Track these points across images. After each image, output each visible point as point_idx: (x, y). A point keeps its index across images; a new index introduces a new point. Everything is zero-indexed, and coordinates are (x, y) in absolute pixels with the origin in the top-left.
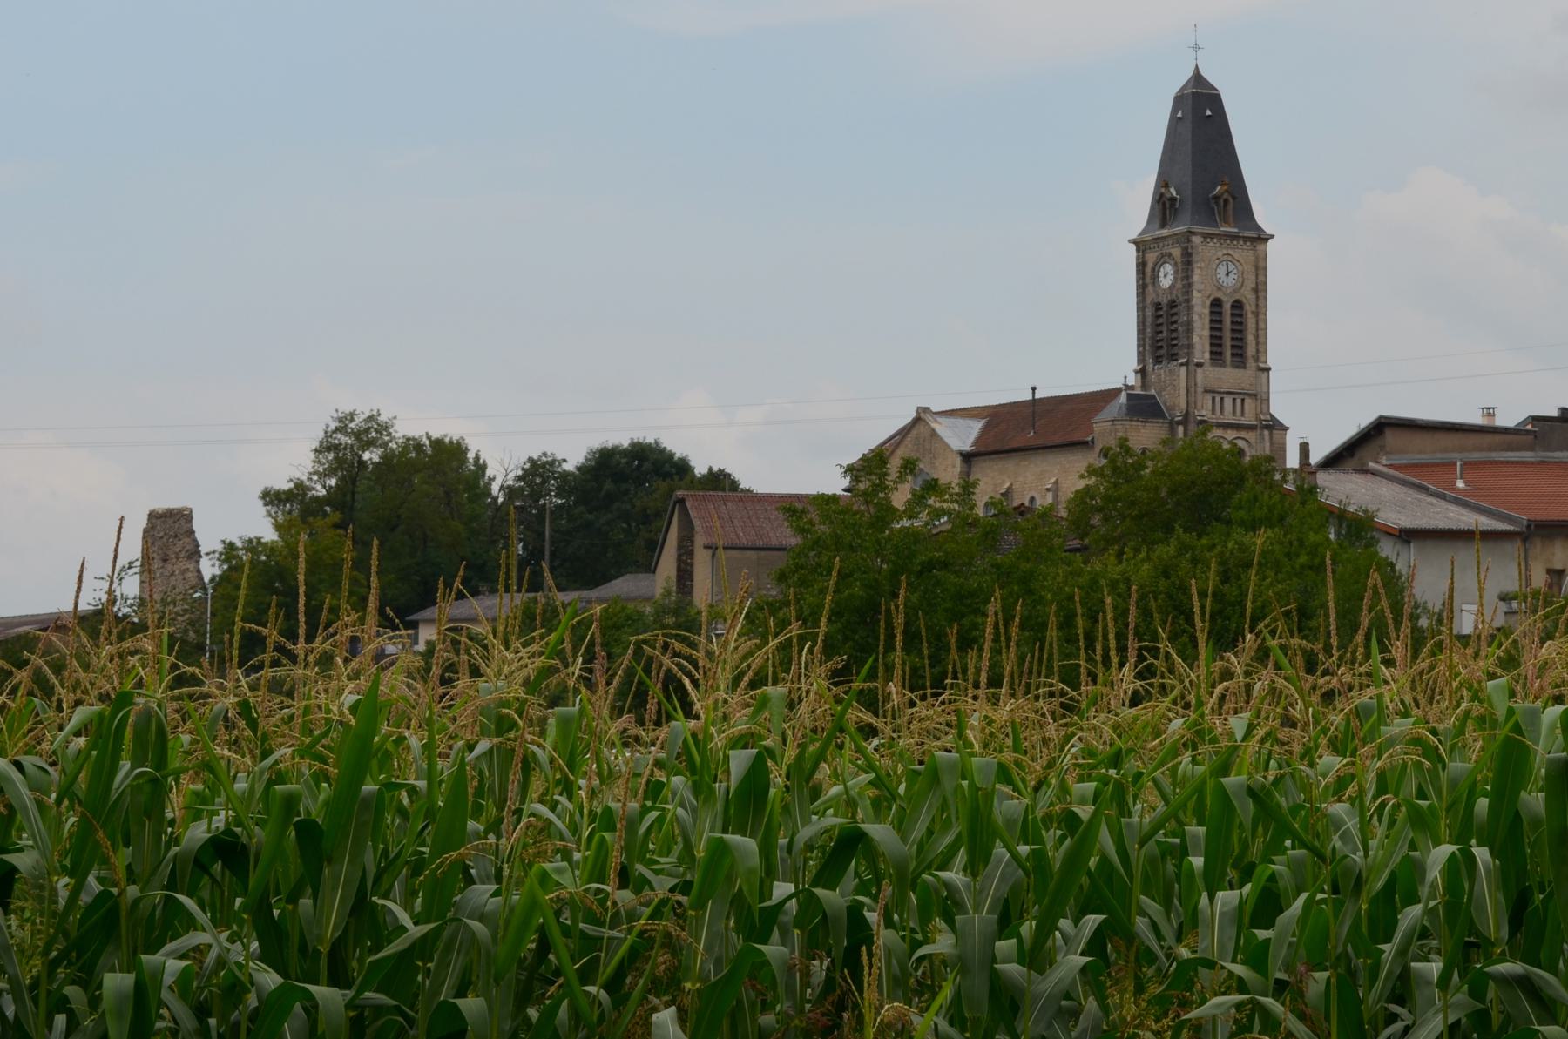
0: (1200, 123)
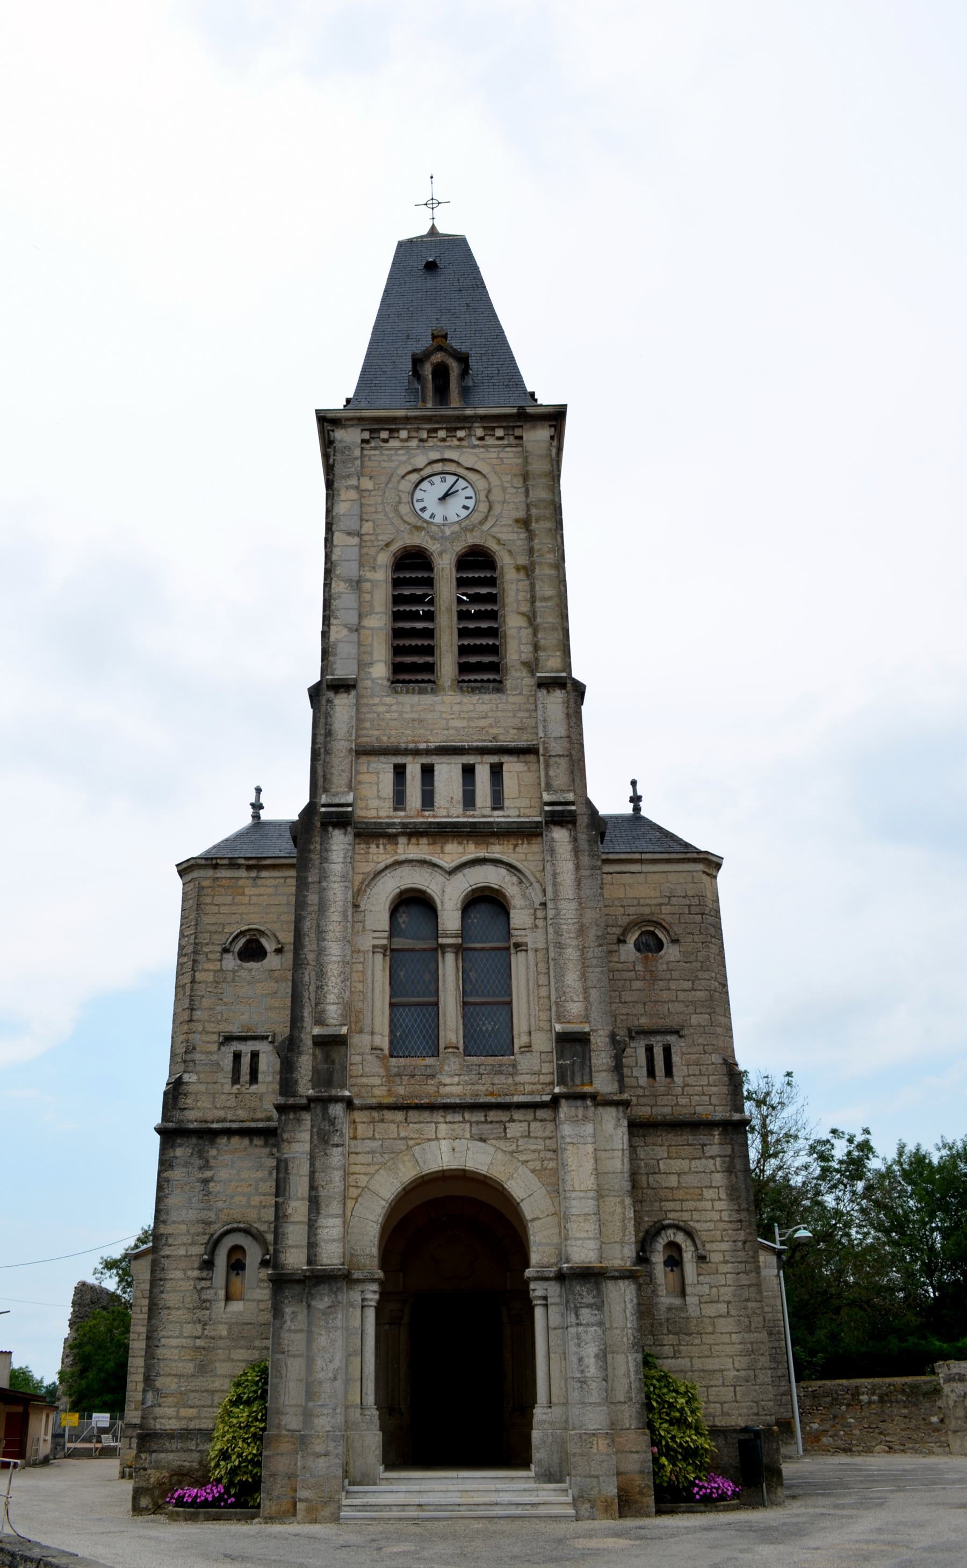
0: (439, 366)
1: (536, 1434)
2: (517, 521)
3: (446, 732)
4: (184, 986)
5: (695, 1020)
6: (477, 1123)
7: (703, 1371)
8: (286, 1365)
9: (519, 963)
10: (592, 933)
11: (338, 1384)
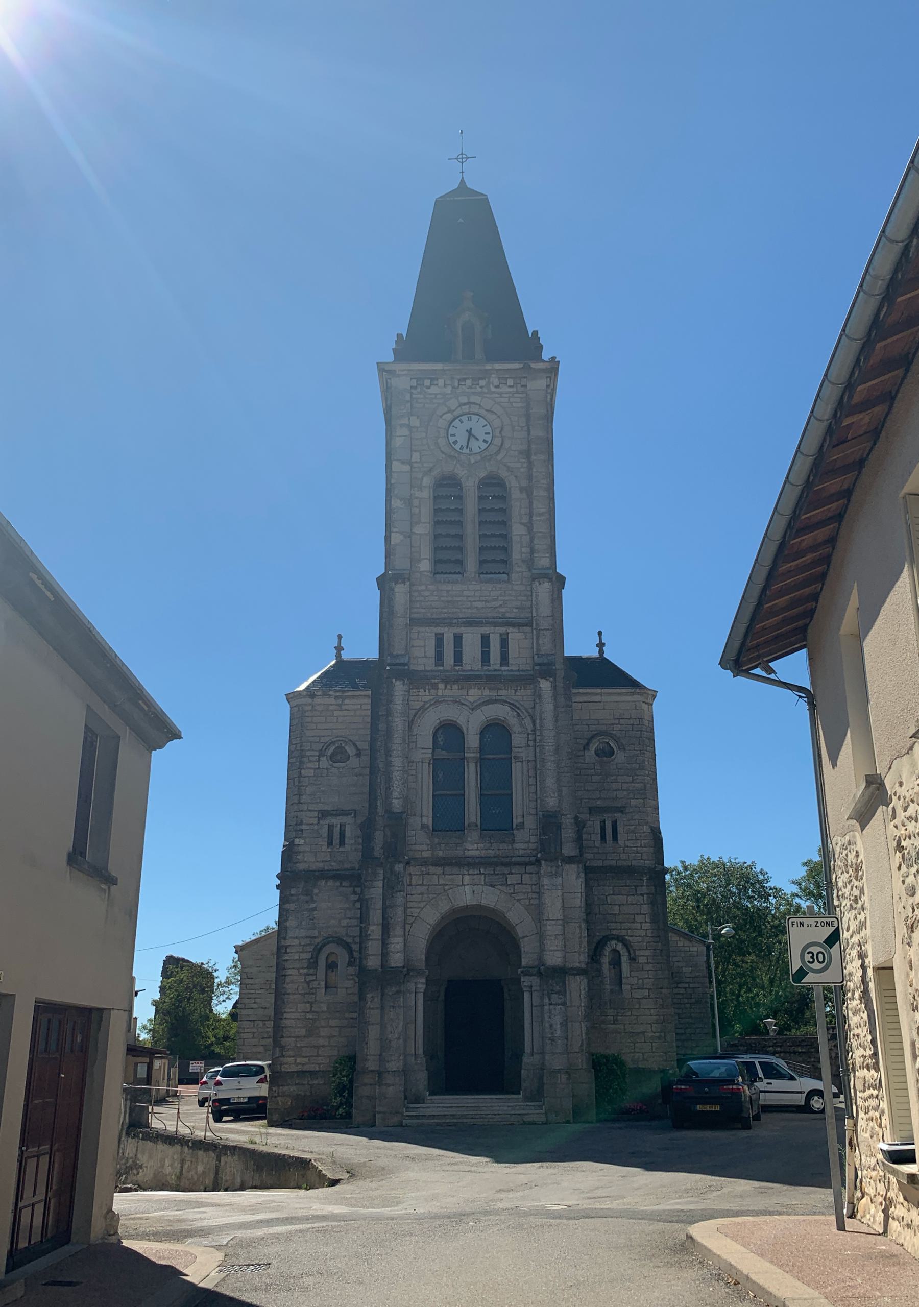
2: (521, 452)
4: (293, 779)
5: (633, 802)
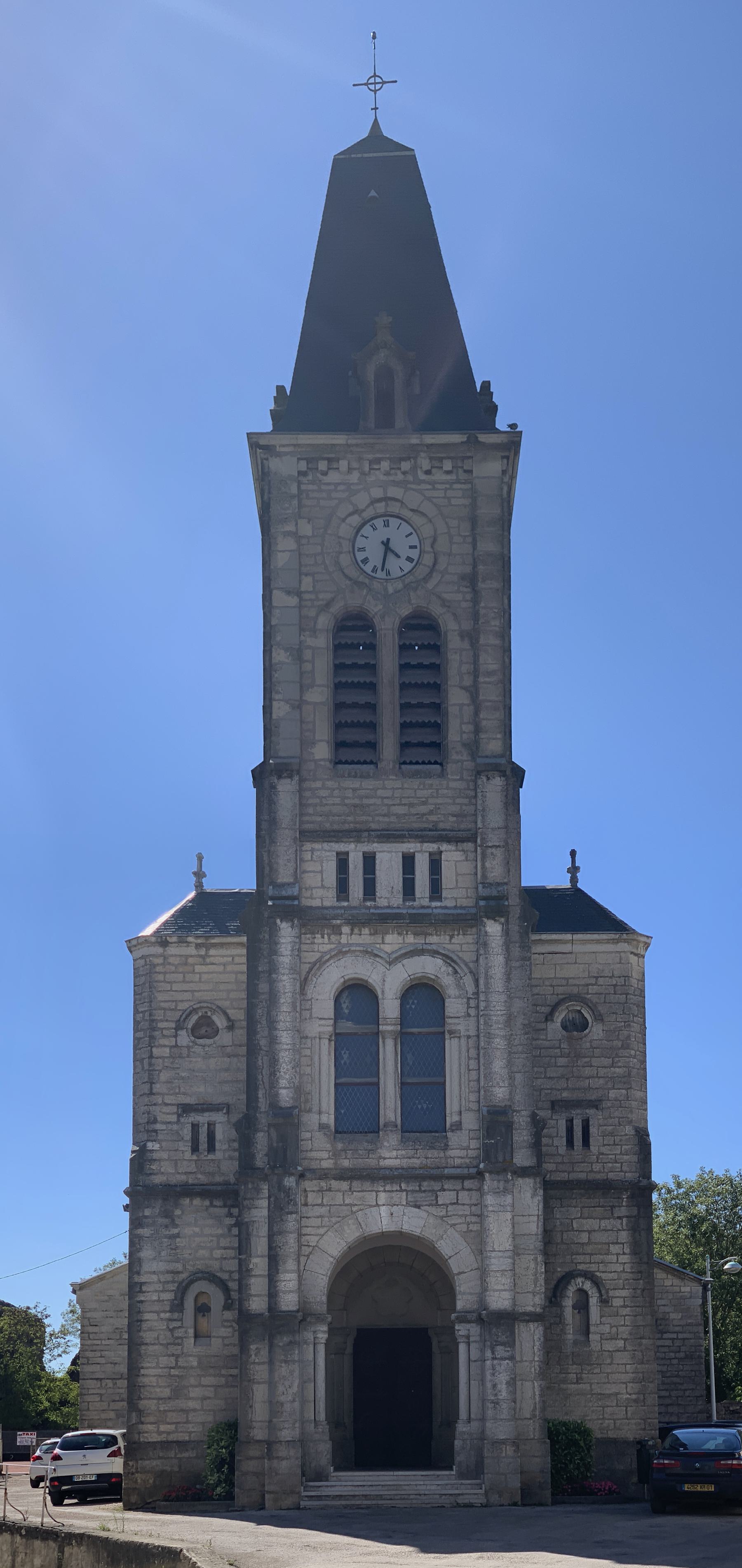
1: (457, 1443)
3: (386, 819)
6: (413, 1191)
7: (601, 1394)
8: (252, 1390)
9: (452, 1048)
10: (520, 1021)
11: (297, 1405)
